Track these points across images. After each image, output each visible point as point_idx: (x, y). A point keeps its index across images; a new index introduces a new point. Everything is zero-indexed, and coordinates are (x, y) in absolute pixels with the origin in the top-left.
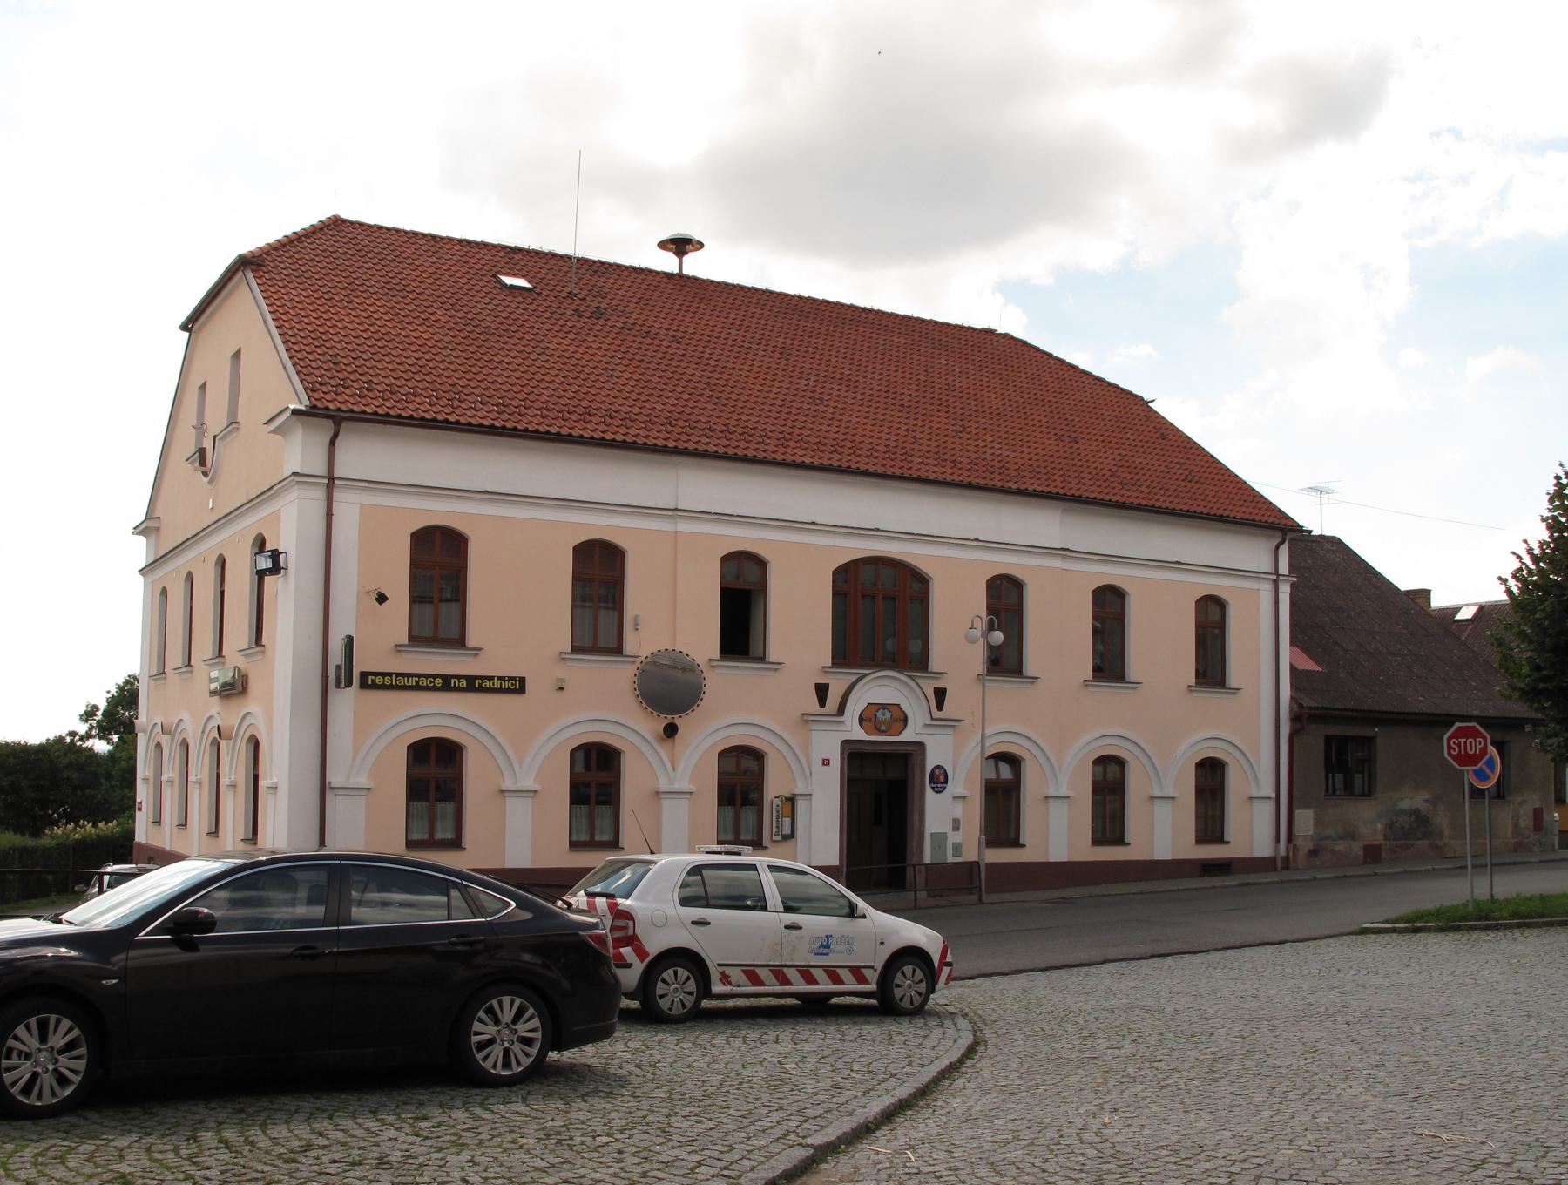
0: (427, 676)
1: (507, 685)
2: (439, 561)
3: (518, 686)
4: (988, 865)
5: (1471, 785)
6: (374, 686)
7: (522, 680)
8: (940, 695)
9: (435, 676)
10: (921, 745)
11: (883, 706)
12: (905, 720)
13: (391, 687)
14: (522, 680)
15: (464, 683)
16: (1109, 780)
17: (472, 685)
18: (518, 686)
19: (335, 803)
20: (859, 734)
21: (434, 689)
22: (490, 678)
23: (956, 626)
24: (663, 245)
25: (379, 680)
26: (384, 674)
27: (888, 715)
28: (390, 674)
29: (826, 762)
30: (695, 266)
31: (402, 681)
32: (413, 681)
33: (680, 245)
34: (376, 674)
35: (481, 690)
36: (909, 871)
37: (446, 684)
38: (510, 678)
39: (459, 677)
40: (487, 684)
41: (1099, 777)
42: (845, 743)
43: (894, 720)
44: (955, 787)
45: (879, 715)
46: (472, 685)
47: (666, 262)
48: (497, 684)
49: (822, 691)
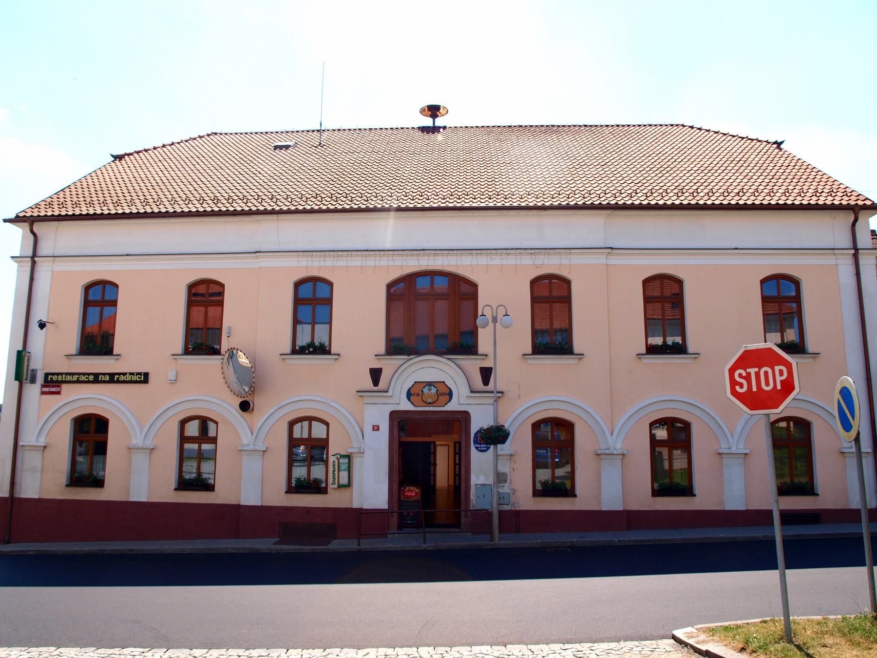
0: (84, 374)
1: (135, 378)
3: (144, 378)
7: (146, 375)
8: (486, 374)
9: (89, 374)
11: (430, 384)
12: (450, 394)
14: (146, 375)
17: (113, 378)
18: (144, 378)
20: (406, 406)
21: (89, 382)
22: (125, 374)
23: (505, 331)
24: (422, 111)
26: (58, 374)
27: (434, 390)
28: (62, 374)
29: (376, 428)
32: (75, 378)
34: (53, 374)
35: (118, 382)
37: (96, 379)
38: (138, 374)
39: (104, 374)
40: (122, 378)
42: (393, 414)
43: (439, 394)
45: (426, 390)
46: (113, 378)
48: (129, 378)
49: (376, 374)
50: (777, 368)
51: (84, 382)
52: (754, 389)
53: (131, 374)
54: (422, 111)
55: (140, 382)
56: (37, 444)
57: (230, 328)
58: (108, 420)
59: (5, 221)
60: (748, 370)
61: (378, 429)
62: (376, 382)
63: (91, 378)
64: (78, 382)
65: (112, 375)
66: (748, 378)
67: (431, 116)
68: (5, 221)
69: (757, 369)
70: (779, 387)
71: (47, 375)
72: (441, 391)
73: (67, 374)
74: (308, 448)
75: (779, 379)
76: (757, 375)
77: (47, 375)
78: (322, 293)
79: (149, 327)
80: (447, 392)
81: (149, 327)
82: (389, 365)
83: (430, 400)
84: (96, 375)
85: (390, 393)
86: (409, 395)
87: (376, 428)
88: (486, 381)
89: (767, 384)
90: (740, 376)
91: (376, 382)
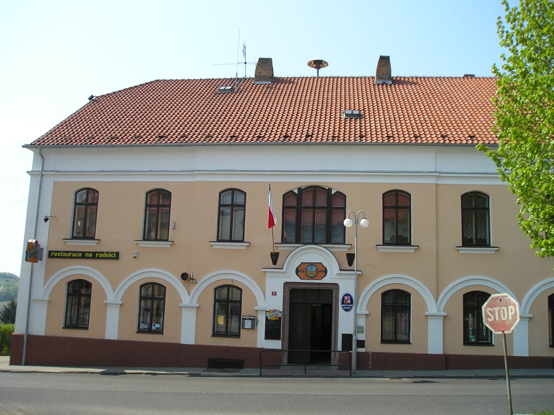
0: (75, 252)
1: (110, 256)
2: (87, 203)
3: (116, 256)
4: (289, 349)
5: (520, 304)
6: (54, 257)
7: (118, 254)
8: (351, 258)
9: (79, 252)
10: (336, 285)
11: (312, 264)
12: (326, 271)
13: (60, 257)
14: (118, 254)
15: (91, 255)
16: (396, 303)
17: (95, 256)
18: (116, 256)
19: (34, 306)
20: (297, 279)
21: (78, 258)
22: (103, 253)
23: (363, 222)
24: (310, 64)
25: (101, 255)
26: (58, 252)
27: (314, 268)
28: (60, 252)
29: (274, 294)
30: (324, 72)
31: (65, 255)
32: (69, 255)
33: (318, 64)
34: (54, 252)
35: (99, 258)
36: (332, 354)
37: (83, 256)
38: (112, 253)
39: (89, 253)
40: (101, 255)
41: (89, 289)
42: (286, 284)
43: (318, 271)
44: (362, 308)
45: (309, 268)
46: (95, 256)
47: (312, 72)
48: (105, 255)
49: (275, 257)
50: (510, 307)
51: (75, 258)
52: (497, 319)
53: (107, 253)
54: (310, 64)
55: (113, 258)
56: (43, 299)
57: (175, 223)
58: (91, 284)
59: (23, 147)
60: (494, 309)
61: (276, 295)
62: (275, 262)
63: (80, 255)
64: (71, 257)
65: (94, 253)
66: (493, 313)
67: (316, 68)
68: (23, 147)
69: (499, 308)
70: (510, 318)
71: (50, 252)
72: (319, 269)
73: (63, 252)
74: (228, 302)
75: (511, 314)
76: (499, 311)
77: (50, 252)
78: (239, 199)
79: (120, 223)
80: (324, 270)
81: (120, 223)
82: (282, 249)
83: (311, 276)
84: (83, 253)
85: (284, 270)
86: (297, 271)
87: (274, 294)
88: (350, 263)
89: (504, 317)
90: (490, 311)
91: (275, 262)
